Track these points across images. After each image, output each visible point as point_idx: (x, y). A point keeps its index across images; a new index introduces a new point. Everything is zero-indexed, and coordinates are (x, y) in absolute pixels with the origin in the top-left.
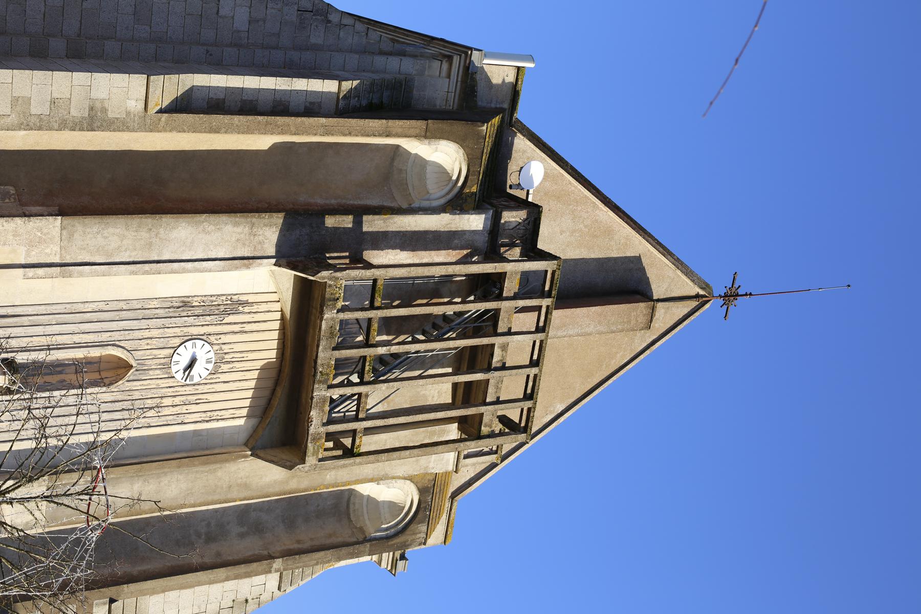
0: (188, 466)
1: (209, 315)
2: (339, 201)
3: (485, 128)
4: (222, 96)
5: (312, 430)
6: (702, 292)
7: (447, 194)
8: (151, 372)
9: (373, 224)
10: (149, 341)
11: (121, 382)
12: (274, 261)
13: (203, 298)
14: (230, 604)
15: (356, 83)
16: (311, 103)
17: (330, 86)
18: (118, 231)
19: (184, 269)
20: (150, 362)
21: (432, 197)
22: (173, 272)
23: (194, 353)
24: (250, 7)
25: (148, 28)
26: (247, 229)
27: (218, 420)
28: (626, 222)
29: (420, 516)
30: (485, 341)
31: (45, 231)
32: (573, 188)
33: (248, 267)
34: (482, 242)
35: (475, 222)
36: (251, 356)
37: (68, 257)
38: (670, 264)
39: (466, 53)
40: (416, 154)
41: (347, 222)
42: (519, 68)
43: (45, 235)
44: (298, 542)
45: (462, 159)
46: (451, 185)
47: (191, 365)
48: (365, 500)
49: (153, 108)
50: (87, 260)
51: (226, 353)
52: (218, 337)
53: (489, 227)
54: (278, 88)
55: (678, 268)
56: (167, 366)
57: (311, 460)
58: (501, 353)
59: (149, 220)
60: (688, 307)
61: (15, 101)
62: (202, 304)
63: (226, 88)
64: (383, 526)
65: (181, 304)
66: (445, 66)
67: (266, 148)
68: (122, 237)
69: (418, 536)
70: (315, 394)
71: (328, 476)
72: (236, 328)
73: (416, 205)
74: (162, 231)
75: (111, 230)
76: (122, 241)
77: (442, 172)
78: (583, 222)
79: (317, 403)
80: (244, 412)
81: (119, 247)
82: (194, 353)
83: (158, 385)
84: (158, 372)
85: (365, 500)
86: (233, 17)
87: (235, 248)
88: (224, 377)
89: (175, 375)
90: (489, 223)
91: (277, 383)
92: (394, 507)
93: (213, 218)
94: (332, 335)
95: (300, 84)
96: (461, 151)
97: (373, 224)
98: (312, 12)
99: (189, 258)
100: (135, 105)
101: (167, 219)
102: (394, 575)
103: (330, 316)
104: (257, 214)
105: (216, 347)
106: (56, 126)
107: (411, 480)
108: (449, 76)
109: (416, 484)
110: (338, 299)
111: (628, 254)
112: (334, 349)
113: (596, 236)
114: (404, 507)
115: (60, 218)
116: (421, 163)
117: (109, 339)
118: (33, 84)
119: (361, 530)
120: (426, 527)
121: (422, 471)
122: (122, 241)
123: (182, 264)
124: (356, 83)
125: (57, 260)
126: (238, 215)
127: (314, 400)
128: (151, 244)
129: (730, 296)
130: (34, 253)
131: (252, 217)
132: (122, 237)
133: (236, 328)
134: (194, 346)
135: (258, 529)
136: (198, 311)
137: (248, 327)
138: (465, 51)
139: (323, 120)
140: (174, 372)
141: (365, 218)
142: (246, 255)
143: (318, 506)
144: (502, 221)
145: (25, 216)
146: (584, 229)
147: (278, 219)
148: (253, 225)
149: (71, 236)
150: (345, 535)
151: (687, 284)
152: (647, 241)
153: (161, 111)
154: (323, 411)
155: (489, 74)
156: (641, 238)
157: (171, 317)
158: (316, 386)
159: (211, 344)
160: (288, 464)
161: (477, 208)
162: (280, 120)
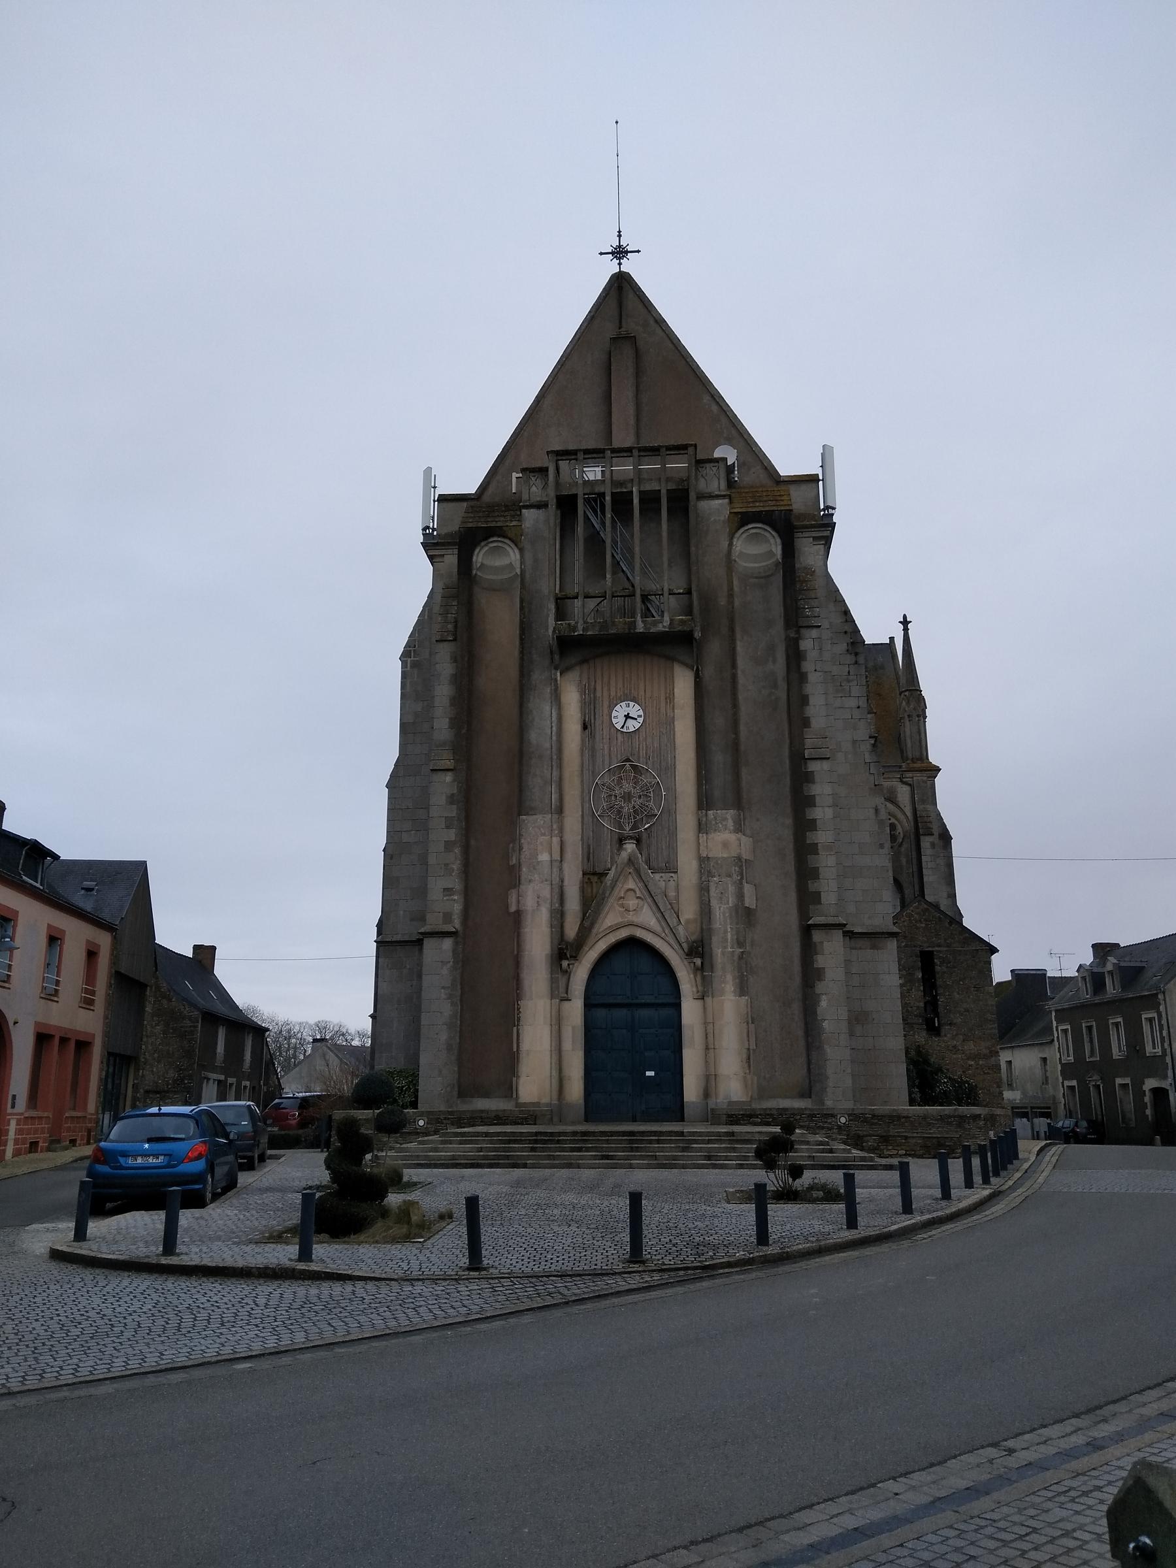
16: (451, 659)
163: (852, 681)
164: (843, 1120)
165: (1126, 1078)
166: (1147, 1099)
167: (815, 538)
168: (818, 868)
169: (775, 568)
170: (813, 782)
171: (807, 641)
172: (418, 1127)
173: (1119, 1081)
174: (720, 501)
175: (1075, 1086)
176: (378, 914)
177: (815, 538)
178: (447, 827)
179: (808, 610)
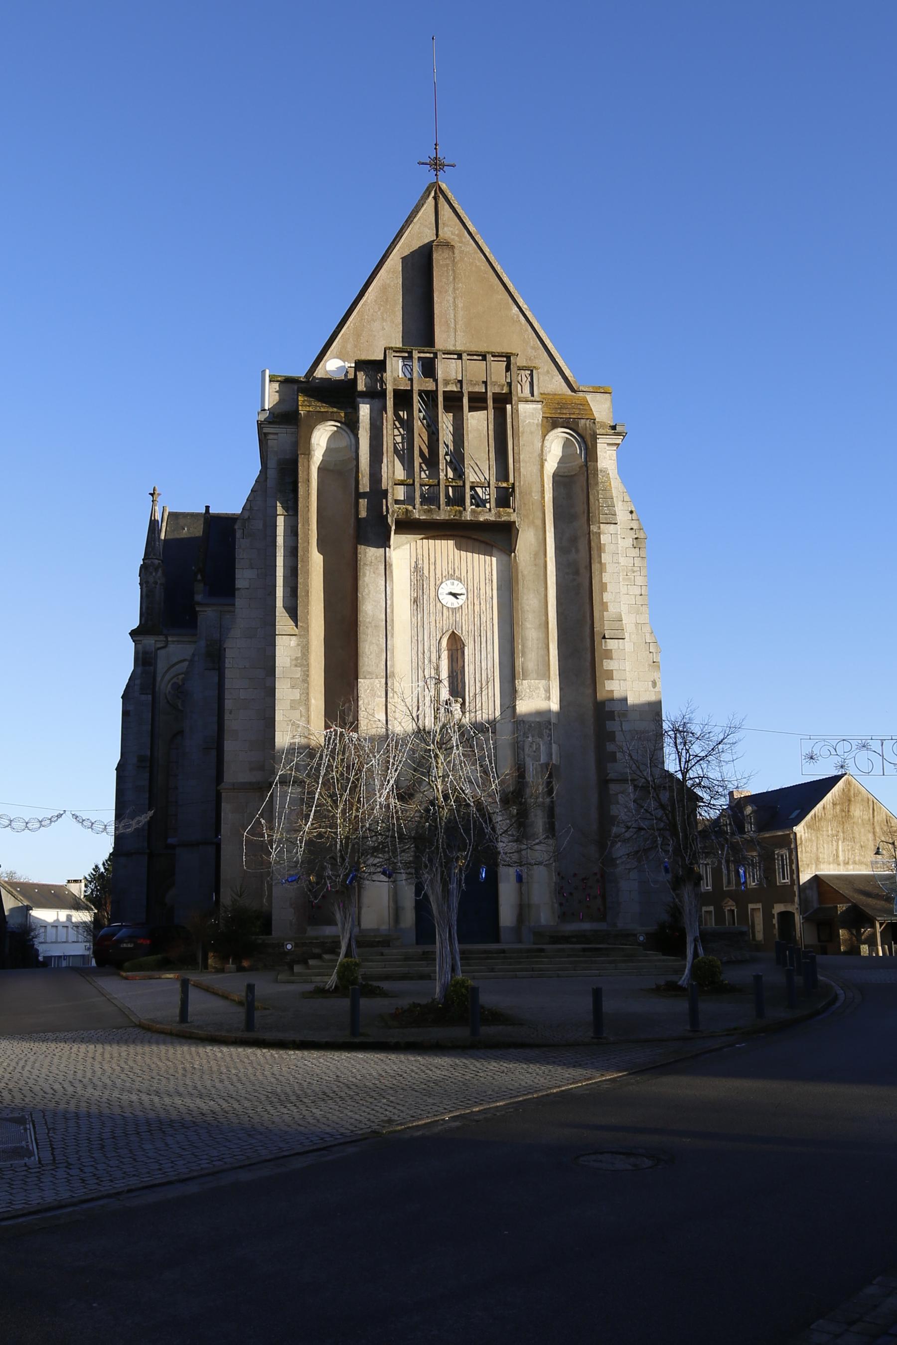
0: (518, 594)
1: (423, 585)
2: (353, 507)
3: (302, 412)
4: (289, 589)
5: (493, 519)
6: (433, 194)
7: (347, 433)
8: (457, 620)
9: (365, 485)
10: (438, 622)
11: (462, 638)
12: (387, 549)
13: (412, 590)
14: (637, 550)
15: (278, 504)
16: (291, 532)
17: (280, 521)
18: (367, 647)
19: (390, 605)
20: (451, 621)
21: (349, 443)
22: (392, 612)
23: (447, 594)
24: (243, 569)
25: (259, 630)
26: (367, 568)
27: (492, 575)
28: (376, 275)
29: (572, 426)
30: (440, 399)
31: (366, 687)
32: (352, 325)
33: (391, 565)
34: (377, 402)
35: (365, 410)
36: (451, 557)
37: (382, 674)
38: (409, 229)
39: (261, 424)
40: (323, 456)
41: (363, 502)
42: (270, 381)
43: (368, 688)
44: (584, 512)
45: (324, 425)
46: (341, 431)
47: (455, 595)
48: (561, 465)
49: (296, 631)
50: (384, 663)
51: (448, 573)
52: (437, 579)
53: (368, 400)
54: (282, 555)
55: (412, 221)
56: (454, 610)
57: (514, 517)
58: (450, 385)
59: (361, 628)
60: (443, 205)
61: (292, 708)
62: (416, 591)
63: (284, 586)
64: (578, 452)
65: (415, 603)
66: (271, 437)
67: (322, 556)
68: (371, 643)
69: (588, 425)
70: (468, 519)
71: (536, 498)
72: (432, 567)
73: (354, 455)
74: (368, 620)
75: (367, 650)
76: (373, 644)
77: (333, 437)
78: (376, 312)
79: (475, 517)
80: (488, 558)
81: (377, 645)
82: (447, 594)
83: (466, 615)
84: (457, 615)
85: (561, 465)
86: (250, 579)
87: (379, 574)
88: (464, 573)
89: (460, 605)
90: (366, 400)
91: (469, 538)
92: (567, 444)
93: (360, 589)
94: (430, 511)
95: (280, 540)
96: (318, 427)
97: (365, 485)
98: (243, 529)
99: (384, 603)
100: (293, 641)
101: (361, 618)
102: (626, 433)
103: (417, 514)
104: (359, 562)
105: (444, 580)
106: (306, 685)
107: (545, 436)
108: (277, 434)
109: (548, 432)
110: (407, 509)
111: (400, 269)
112: (439, 509)
113: (387, 299)
114: (567, 438)
115: (359, 680)
116: (328, 451)
117: (435, 646)
118: (283, 699)
119: (581, 467)
120: (582, 420)
121: (540, 428)
122: (373, 644)
123: (388, 606)
124: (278, 504)
125: (384, 680)
126: (358, 574)
127: (473, 519)
128: (376, 626)
129: (437, 165)
130: (379, 694)
131: (360, 565)
132: (371, 643)
133: (432, 567)
134: (442, 594)
135: (574, 540)
136: (420, 592)
137: (432, 560)
138: (260, 425)
139: (300, 526)
140: (458, 606)
141: (361, 490)
142: (383, 567)
143: (564, 498)
144: (365, 389)
145: (358, 699)
146: (381, 311)
147: (361, 548)
148: (365, 564)
149: (369, 673)
150: (583, 479)
151: (425, 210)
152: (392, 251)
153: (297, 626)
154: (480, 512)
155: (275, 403)
156: (389, 260)
157: (423, 610)
158: (463, 518)
159: (442, 583)
160: (516, 532)
161: (356, 410)
162: (300, 553)
163: (636, 571)
164: (641, 938)
165: (758, 904)
166: (775, 921)
167: (609, 444)
168: (614, 732)
169: (578, 469)
170: (611, 659)
171: (606, 535)
172: (286, 950)
173: (751, 906)
174: (534, 406)
175: (712, 911)
176: (117, 757)
177: (609, 444)
178: (293, 687)
179: (606, 508)
